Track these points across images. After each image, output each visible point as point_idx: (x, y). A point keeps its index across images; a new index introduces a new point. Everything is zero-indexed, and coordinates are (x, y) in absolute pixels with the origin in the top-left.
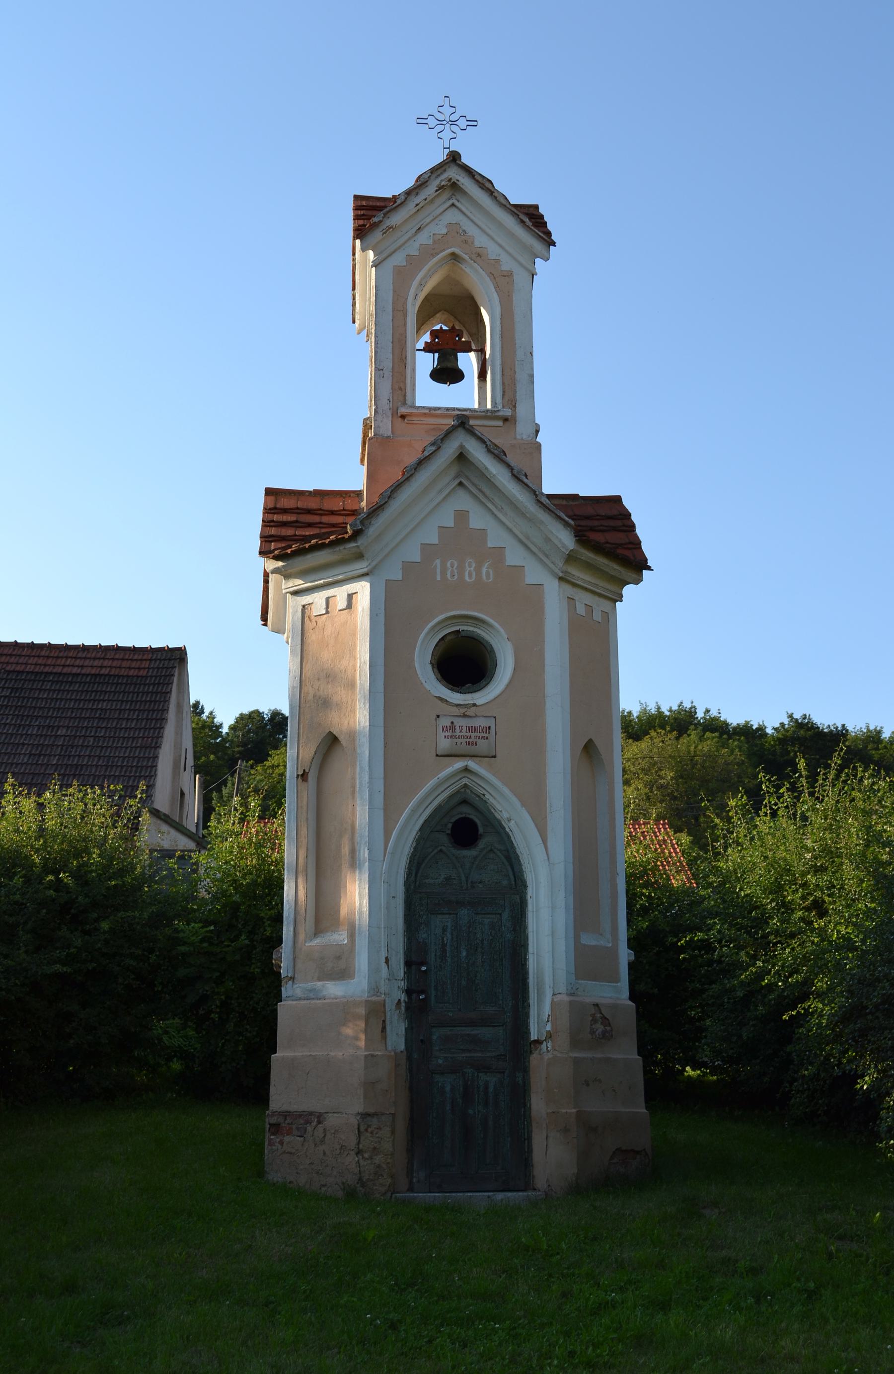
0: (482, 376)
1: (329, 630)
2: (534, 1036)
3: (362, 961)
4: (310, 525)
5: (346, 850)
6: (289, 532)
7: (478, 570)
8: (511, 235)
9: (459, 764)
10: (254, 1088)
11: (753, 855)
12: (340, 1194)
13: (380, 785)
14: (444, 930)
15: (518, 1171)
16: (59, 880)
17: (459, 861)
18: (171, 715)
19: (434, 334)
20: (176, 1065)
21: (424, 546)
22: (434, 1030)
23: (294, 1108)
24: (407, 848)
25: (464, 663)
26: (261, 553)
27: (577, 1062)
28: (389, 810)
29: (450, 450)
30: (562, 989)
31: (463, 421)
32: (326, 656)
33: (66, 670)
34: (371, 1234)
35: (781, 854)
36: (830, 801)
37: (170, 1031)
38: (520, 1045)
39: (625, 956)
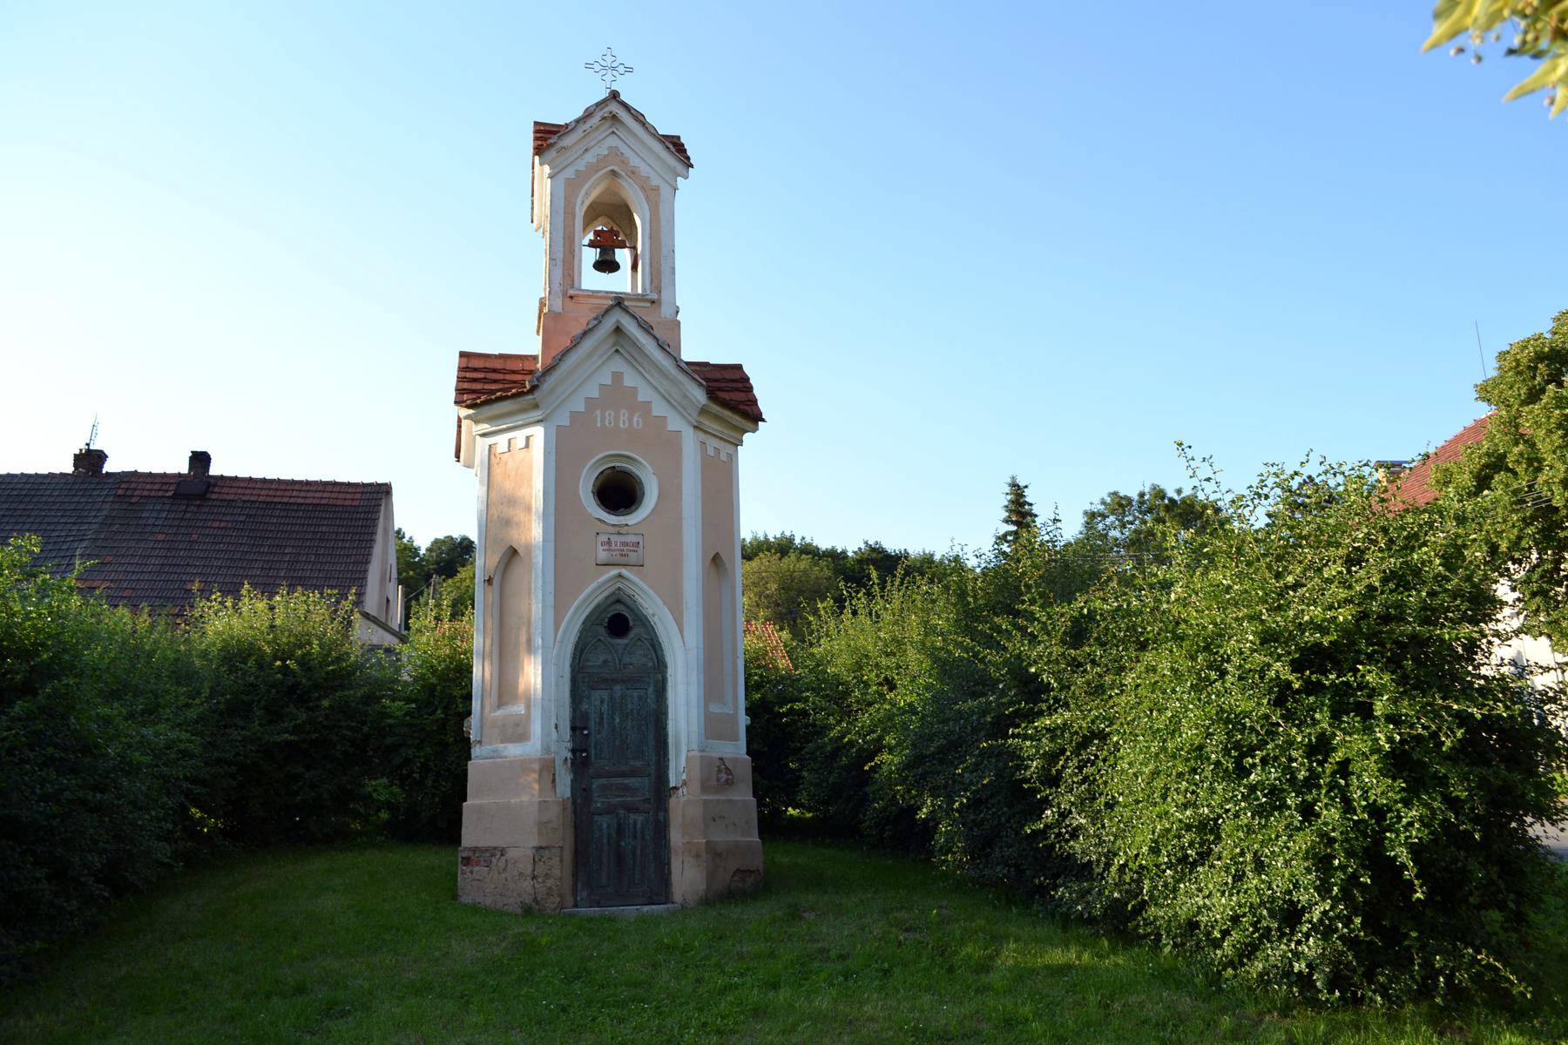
0: (634, 267)
1: (511, 465)
2: (672, 784)
3: (536, 728)
4: (495, 381)
5: (523, 639)
6: (478, 386)
7: (630, 419)
8: (659, 158)
9: (614, 571)
10: (449, 831)
11: (837, 645)
12: (519, 911)
13: (551, 588)
14: (602, 702)
15: (660, 889)
16: (287, 667)
17: (613, 648)
18: (379, 537)
19: (597, 233)
20: (384, 815)
21: (588, 400)
23: (482, 844)
25: (618, 492)
26: (456, 402)
27: (706, 802)
28: (559, 608)
29: (609, 324)
30: (695, 746)
31: (619, 302)
32: (508, 485)
34: (544, 941)
35: (861, 642)
36: (896, 604)
37: (379, 787)
38: (661, 791)
39: (743, 720)
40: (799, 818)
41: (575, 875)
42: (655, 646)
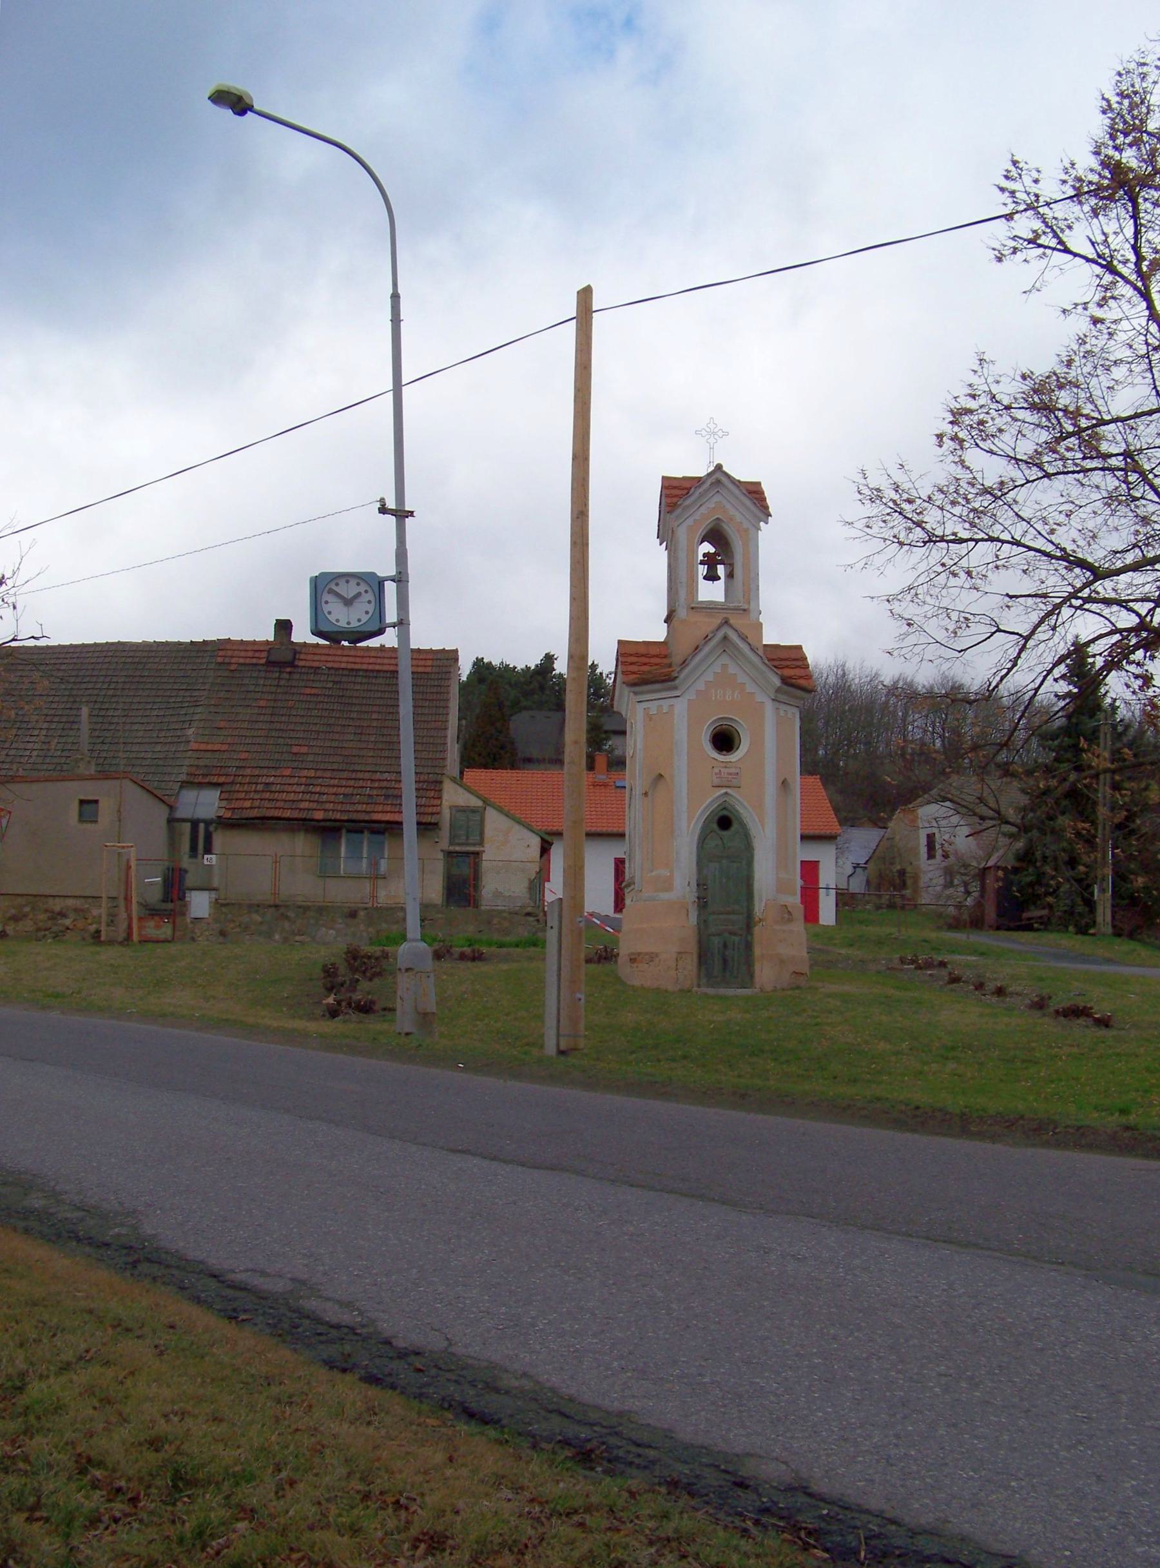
8: (748, 509)
9: (723, 791)
24: (698, 831)
29: (720, 635)
33: (371, 667)
41: (699, 970)
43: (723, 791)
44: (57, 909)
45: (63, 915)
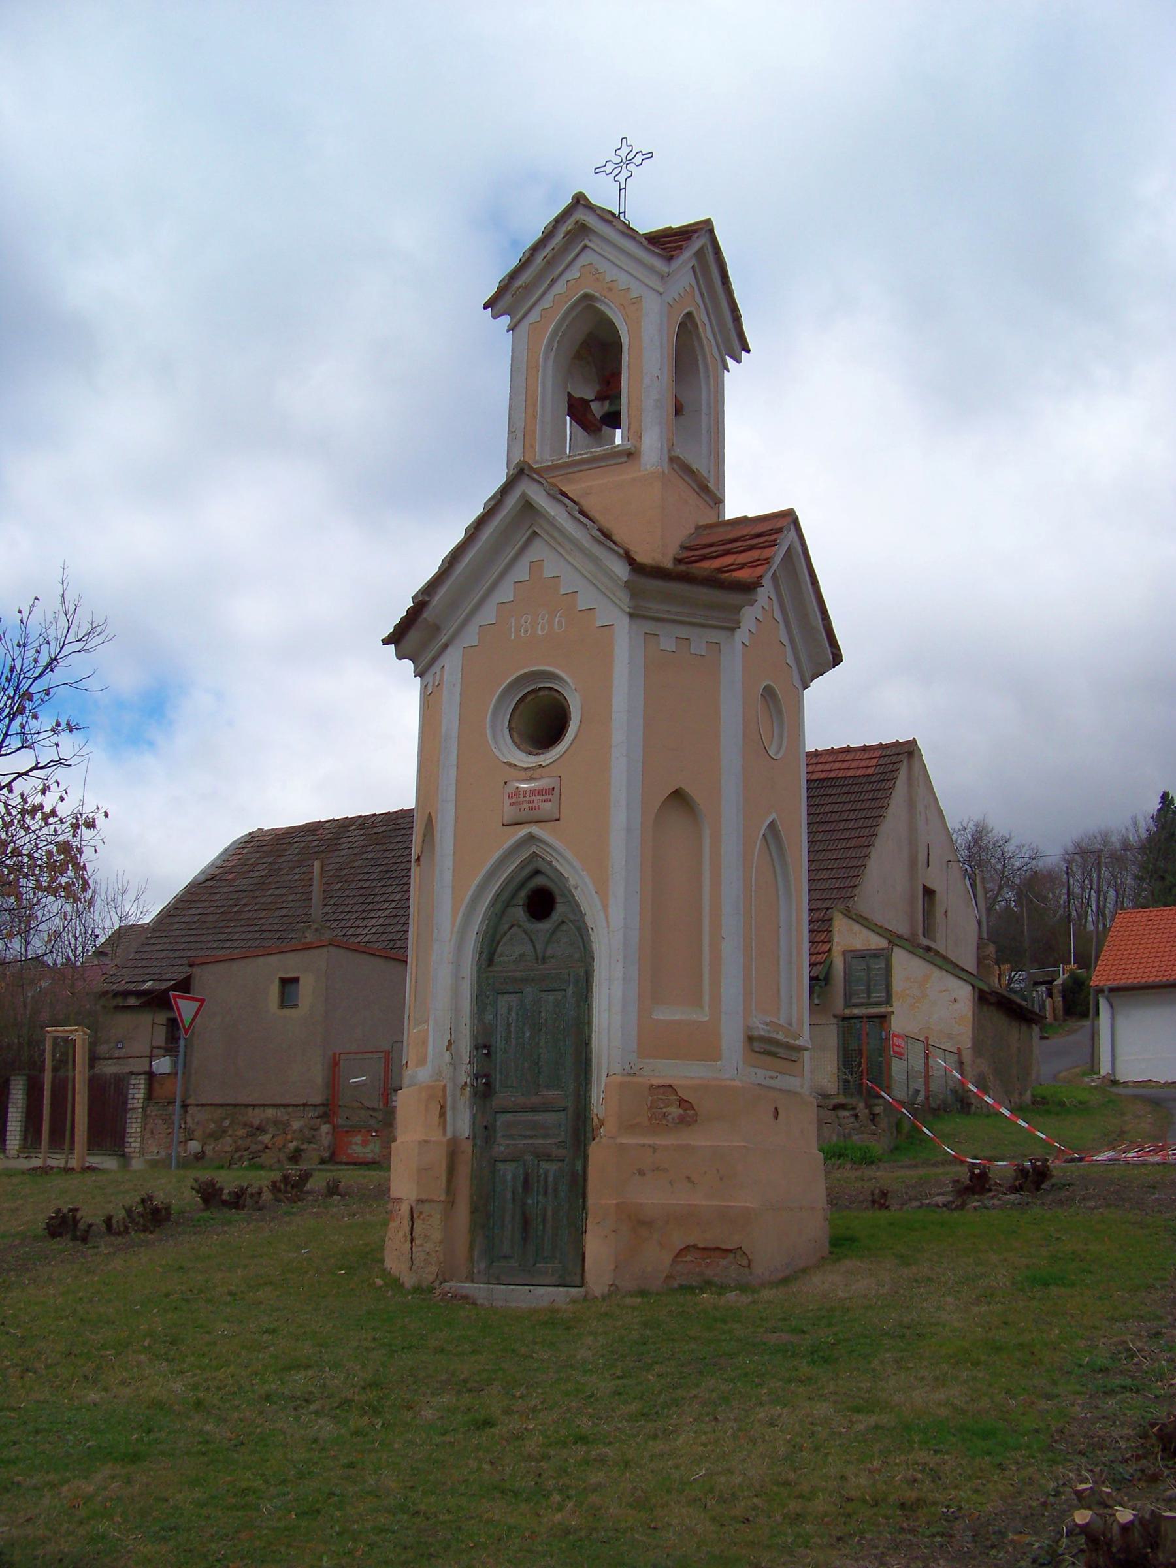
8: (639, 261)
9: (523, 831)
14: (510, 1010)
22: (498, 1115)
25: (543, 720)
40: (1018, 1117)
42: (582, 934)
43: (523, 831)
44: (256, 1123)
45: (261, 1129)
